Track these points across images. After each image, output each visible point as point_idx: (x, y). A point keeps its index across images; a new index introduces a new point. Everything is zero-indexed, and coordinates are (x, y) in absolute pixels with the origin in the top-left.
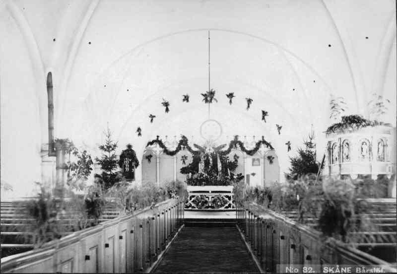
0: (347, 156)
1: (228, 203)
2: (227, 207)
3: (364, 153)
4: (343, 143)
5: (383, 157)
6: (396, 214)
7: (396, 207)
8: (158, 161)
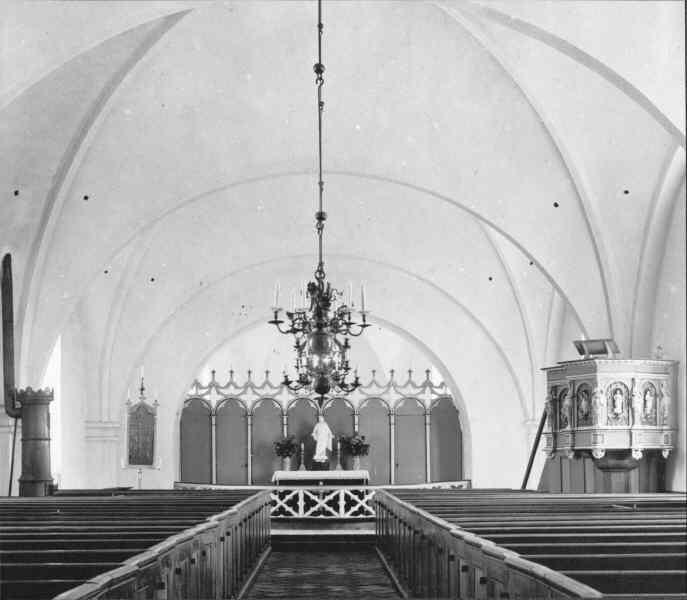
0: (586, 415)
1: (285, 500)
2: (355, 513)
3: (618, 410)
4: (579, 390)
5: (654, 416)
6: (685, 521)
7: (685, 508)
8: (249, 422)
